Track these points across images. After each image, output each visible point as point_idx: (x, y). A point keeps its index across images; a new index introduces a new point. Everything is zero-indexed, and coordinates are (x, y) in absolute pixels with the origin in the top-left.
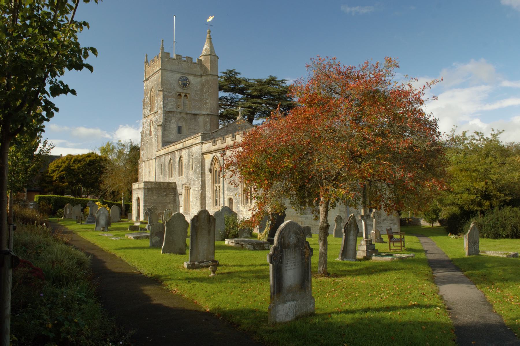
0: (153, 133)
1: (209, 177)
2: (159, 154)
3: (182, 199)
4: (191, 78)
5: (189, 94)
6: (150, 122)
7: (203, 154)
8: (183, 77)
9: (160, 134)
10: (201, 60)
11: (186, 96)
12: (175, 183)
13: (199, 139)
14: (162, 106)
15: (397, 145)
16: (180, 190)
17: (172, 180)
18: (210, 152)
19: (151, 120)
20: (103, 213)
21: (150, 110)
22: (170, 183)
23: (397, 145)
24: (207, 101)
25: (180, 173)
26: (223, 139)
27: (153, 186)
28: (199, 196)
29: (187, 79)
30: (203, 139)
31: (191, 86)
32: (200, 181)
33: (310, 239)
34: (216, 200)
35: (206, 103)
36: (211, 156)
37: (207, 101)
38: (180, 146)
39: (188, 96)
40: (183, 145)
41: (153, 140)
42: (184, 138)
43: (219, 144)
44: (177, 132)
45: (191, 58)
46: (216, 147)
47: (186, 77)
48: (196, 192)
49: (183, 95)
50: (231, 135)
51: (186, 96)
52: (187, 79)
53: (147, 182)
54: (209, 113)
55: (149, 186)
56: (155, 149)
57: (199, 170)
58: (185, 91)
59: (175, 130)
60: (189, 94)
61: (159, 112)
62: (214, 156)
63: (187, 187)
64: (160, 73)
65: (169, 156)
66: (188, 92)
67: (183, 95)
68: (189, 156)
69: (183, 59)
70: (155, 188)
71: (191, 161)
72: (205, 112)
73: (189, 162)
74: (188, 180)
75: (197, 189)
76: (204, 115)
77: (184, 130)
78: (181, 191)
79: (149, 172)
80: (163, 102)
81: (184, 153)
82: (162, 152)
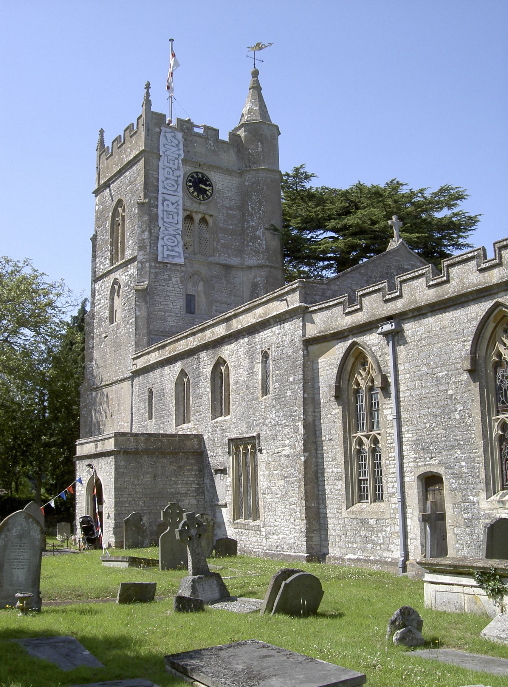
0: (119, 316)
1: (332, 417)
2: (141, 363)
3: (224, 487)
4: (215, 177)
5: (211, 216)
6: (113, 288)
7: (308, 343)
8: (197, 173)
9: (143, 313)
10: (239, 136)
11: (203, 220)
12: (199, 438)
13: (295, 301)
14: (147, 242)
15: (172, 460)
16: (219, 456)
17: (186, 429)
18: (339, 336)
19: (116, 282)
20: (21, 537)
21: (111, 260)
22: (186, 437)
23: (172, 460)
24: (258, 233)
25: (220, 404)
26: (392, 287)
27: (142, 446)
28: (297, 472)
29: (205, 180)
30: (303, 299)
31: (216, 195)
32: (300, 425)
33: (225, 561)
34: (360, 481)
35: (255, 238)
36: (339, 349)
37: (258, 233)
38: (221, 331)
39: (210, 220)
40: (227, 329)
41: (122, 330)
42: (230, 305)
43: (373, 306)
44: (183, 312)
45: (217, 131)
46: (360, 318)
47: (203, 175)
48: (284, 461)
49: (197, 218)
50: (344, 298)
51: (203, 220)
52: (208, 179)
53: (124, 434)
54: (262, 262)
55: (132, 446)
56: (130, 350)
57: (295, 393)
58: (202, 208)
59: (179, 304)
60: (211, 216)
61: (140, 258)
62: (354, 344)
63: (245, 448)
64: (142, 161)
65: (178, 366)
66: (210, 212)
67: (197, 218)
68: (251, 356)
69: (196, 130)
70: (147, 451)
71: (259, 368)
72: (252, 261)
73: (251, 372)
74: (250, 427)
75: (287, 451)
76: (250, 268)
77: (201, 301)
78: (220, 459)
79: (124, 408)
80: (150, 232)
81: (227, 351)
82: (154, 357)
